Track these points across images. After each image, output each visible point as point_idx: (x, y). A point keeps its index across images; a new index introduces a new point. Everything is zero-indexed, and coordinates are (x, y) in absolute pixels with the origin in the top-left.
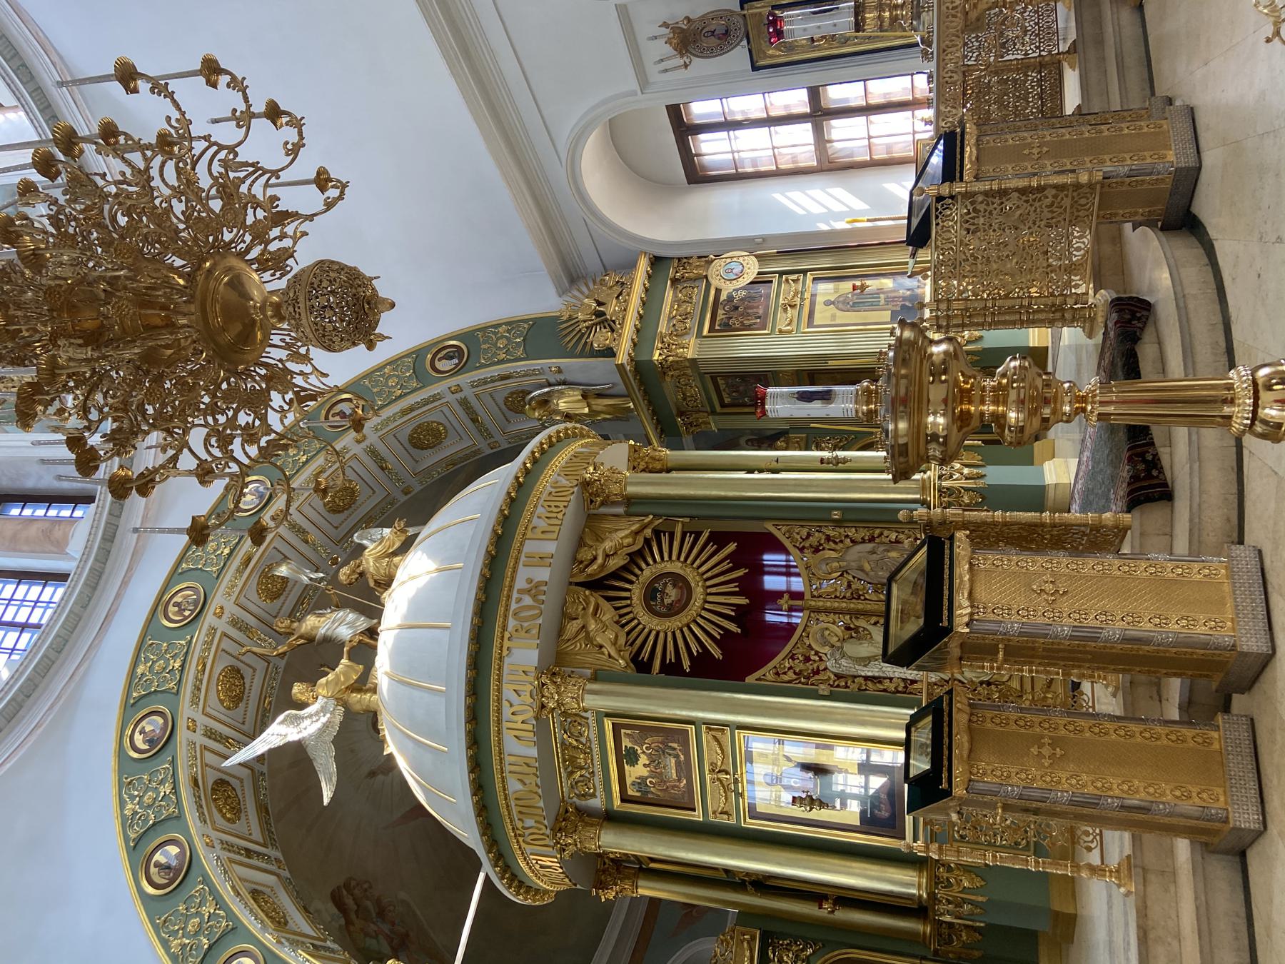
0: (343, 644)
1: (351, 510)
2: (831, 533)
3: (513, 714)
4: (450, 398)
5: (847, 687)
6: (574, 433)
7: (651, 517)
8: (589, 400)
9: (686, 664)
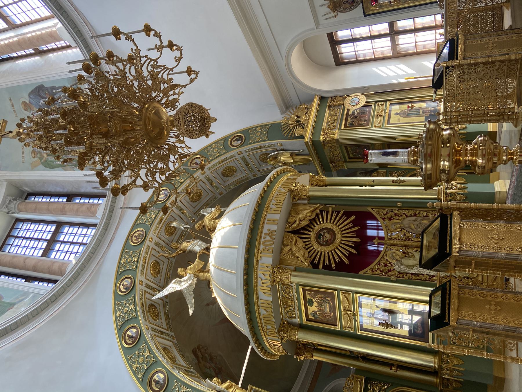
0: (197, 253)
1: (199, 201)
2: (397, 212)
4: (237, 156)
5: (403, 277)
6: (284, 171)
8: (293, 157)
9: (333, 266)
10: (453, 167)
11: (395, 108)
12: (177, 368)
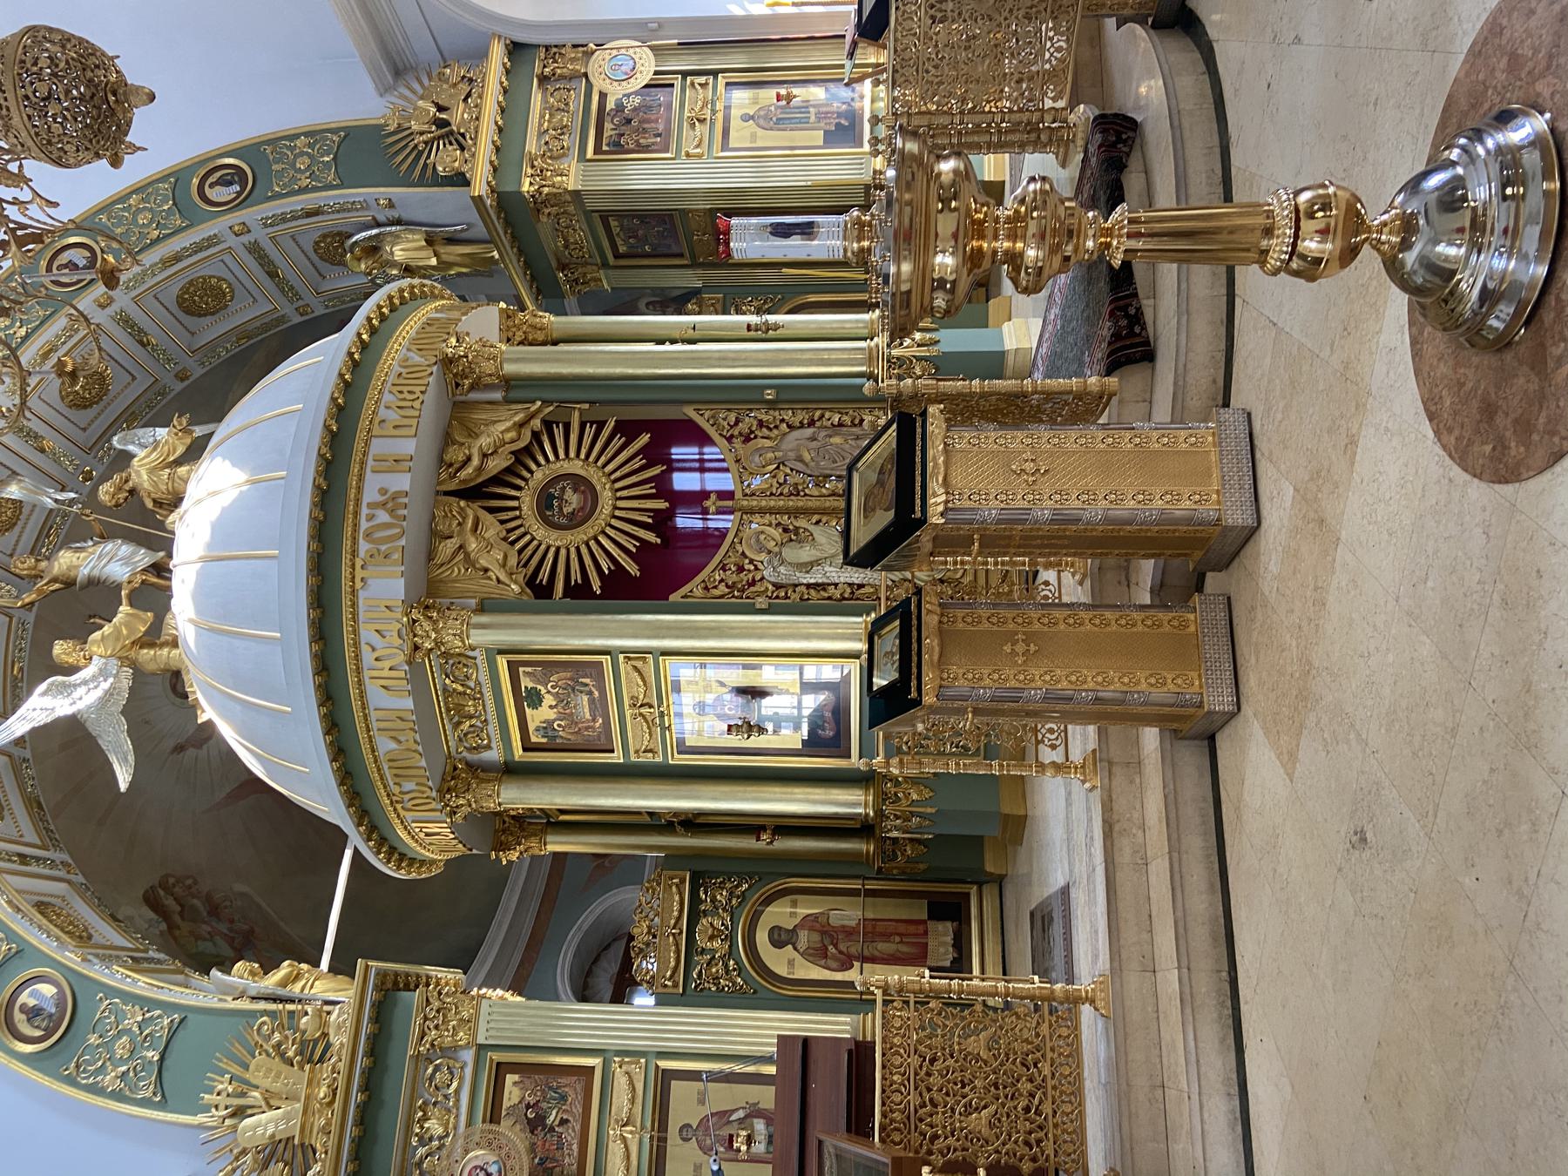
0: (119, 587)
1: (102, 404)
2: (765, 418)
3: (376, 659)
4: (232, 241)
5: (787, 597)
6: (412, 293)
7: (539, 403)
8: (437, 248)
9: (596, 585)
10: (965, 271)
11: (741, 98)
12: (102, 958)
